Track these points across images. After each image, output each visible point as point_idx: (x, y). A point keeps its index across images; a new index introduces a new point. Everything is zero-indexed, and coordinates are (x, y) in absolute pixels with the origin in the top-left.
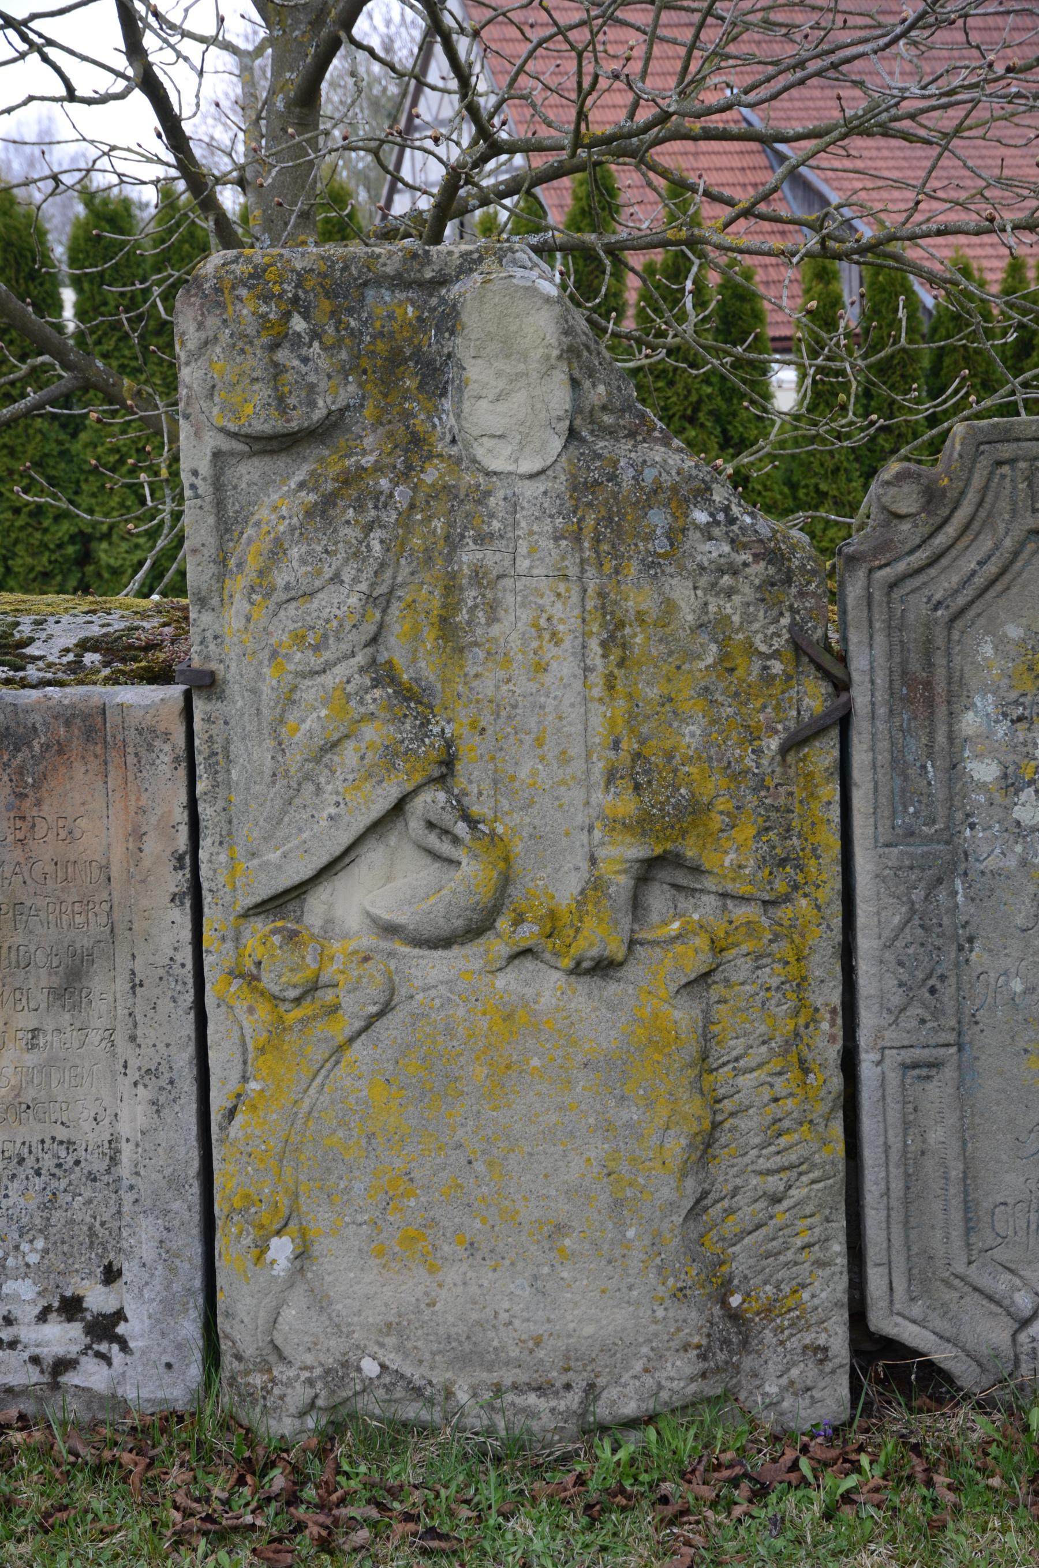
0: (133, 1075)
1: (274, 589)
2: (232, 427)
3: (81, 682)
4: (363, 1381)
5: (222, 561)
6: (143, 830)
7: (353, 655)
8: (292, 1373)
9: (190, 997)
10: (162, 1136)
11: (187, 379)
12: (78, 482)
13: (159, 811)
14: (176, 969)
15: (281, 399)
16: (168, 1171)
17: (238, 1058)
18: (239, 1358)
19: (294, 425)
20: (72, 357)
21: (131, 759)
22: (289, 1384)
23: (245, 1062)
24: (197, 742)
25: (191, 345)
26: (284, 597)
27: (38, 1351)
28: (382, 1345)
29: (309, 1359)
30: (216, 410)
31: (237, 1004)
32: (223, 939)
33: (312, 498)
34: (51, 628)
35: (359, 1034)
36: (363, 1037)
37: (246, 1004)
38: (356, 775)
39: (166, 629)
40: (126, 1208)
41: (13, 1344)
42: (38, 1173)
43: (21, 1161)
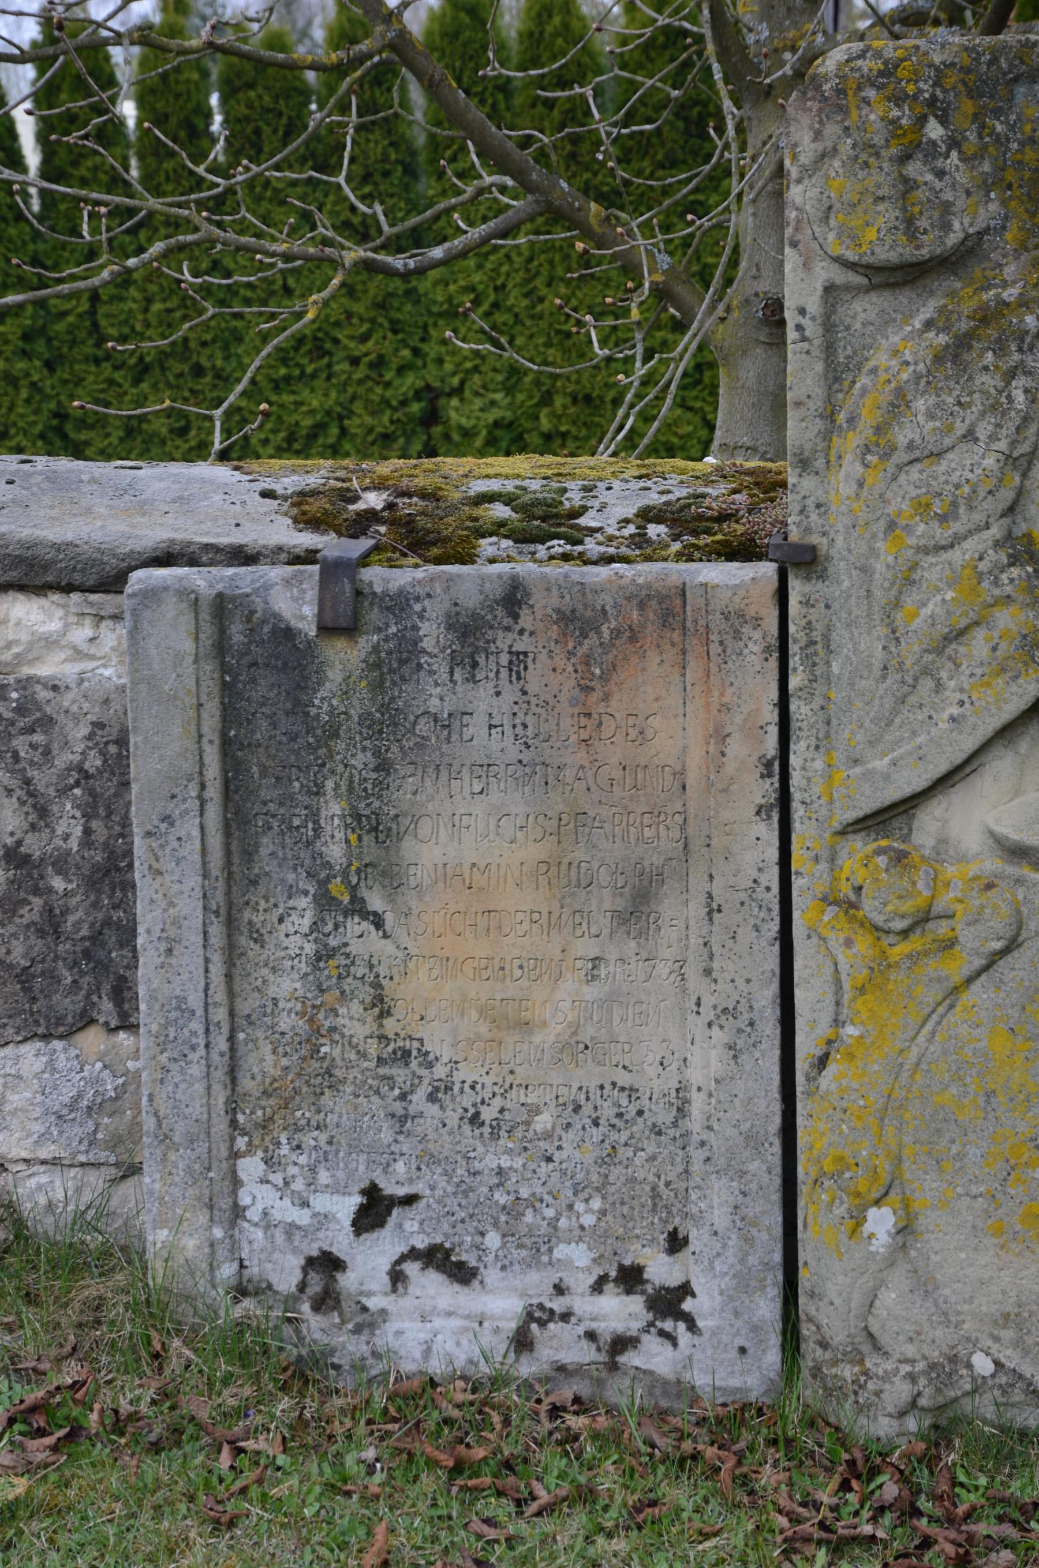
0: (708, 1013)
1: (893, 448)
2: (851, 256)
3: (648, 559)
4: (974, 1379)
5: (829, 416)
6: (727, 730)
7: (987, 526)
8: (889, 1366)
9: (775, 926)
10: (739, 1086)
11: (798, 200)
12: (425, 327)
13: (745, 709)
14: (760, 893)
15: (910, 221)
16: (745, 1126)
17: (830, 999)
18: (824, 1345)
19: (925, 252)
20: (534, 177)
21: (715, 648)
22: (886, 1378)
23: (838, 1004)
24: (792, 629)
25: (805, 159)
26: (906, 457)
27: (594, 1325)
28: (997, 1339)
29: (910, 1351)
30: (831, 236)
31: (831, 935)
32: (817, 859)
33: (943, 339)
34: (604, 496)
35: (979, 973)
36: (984, 977)
37: (842, 936)
38: (986, 669)
39: (737, 496)
40: (696, 1167)
41: (566, 1317)
42: (596, 1123)
43: (577, 1109)
